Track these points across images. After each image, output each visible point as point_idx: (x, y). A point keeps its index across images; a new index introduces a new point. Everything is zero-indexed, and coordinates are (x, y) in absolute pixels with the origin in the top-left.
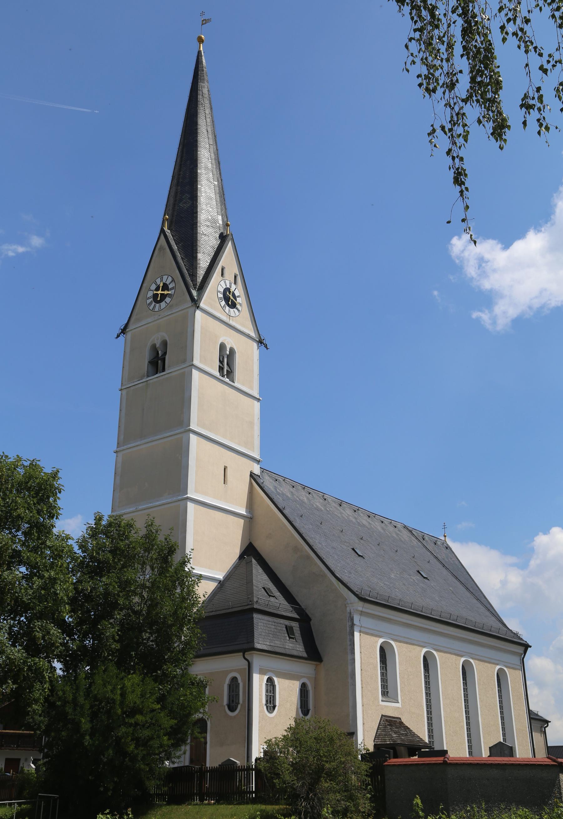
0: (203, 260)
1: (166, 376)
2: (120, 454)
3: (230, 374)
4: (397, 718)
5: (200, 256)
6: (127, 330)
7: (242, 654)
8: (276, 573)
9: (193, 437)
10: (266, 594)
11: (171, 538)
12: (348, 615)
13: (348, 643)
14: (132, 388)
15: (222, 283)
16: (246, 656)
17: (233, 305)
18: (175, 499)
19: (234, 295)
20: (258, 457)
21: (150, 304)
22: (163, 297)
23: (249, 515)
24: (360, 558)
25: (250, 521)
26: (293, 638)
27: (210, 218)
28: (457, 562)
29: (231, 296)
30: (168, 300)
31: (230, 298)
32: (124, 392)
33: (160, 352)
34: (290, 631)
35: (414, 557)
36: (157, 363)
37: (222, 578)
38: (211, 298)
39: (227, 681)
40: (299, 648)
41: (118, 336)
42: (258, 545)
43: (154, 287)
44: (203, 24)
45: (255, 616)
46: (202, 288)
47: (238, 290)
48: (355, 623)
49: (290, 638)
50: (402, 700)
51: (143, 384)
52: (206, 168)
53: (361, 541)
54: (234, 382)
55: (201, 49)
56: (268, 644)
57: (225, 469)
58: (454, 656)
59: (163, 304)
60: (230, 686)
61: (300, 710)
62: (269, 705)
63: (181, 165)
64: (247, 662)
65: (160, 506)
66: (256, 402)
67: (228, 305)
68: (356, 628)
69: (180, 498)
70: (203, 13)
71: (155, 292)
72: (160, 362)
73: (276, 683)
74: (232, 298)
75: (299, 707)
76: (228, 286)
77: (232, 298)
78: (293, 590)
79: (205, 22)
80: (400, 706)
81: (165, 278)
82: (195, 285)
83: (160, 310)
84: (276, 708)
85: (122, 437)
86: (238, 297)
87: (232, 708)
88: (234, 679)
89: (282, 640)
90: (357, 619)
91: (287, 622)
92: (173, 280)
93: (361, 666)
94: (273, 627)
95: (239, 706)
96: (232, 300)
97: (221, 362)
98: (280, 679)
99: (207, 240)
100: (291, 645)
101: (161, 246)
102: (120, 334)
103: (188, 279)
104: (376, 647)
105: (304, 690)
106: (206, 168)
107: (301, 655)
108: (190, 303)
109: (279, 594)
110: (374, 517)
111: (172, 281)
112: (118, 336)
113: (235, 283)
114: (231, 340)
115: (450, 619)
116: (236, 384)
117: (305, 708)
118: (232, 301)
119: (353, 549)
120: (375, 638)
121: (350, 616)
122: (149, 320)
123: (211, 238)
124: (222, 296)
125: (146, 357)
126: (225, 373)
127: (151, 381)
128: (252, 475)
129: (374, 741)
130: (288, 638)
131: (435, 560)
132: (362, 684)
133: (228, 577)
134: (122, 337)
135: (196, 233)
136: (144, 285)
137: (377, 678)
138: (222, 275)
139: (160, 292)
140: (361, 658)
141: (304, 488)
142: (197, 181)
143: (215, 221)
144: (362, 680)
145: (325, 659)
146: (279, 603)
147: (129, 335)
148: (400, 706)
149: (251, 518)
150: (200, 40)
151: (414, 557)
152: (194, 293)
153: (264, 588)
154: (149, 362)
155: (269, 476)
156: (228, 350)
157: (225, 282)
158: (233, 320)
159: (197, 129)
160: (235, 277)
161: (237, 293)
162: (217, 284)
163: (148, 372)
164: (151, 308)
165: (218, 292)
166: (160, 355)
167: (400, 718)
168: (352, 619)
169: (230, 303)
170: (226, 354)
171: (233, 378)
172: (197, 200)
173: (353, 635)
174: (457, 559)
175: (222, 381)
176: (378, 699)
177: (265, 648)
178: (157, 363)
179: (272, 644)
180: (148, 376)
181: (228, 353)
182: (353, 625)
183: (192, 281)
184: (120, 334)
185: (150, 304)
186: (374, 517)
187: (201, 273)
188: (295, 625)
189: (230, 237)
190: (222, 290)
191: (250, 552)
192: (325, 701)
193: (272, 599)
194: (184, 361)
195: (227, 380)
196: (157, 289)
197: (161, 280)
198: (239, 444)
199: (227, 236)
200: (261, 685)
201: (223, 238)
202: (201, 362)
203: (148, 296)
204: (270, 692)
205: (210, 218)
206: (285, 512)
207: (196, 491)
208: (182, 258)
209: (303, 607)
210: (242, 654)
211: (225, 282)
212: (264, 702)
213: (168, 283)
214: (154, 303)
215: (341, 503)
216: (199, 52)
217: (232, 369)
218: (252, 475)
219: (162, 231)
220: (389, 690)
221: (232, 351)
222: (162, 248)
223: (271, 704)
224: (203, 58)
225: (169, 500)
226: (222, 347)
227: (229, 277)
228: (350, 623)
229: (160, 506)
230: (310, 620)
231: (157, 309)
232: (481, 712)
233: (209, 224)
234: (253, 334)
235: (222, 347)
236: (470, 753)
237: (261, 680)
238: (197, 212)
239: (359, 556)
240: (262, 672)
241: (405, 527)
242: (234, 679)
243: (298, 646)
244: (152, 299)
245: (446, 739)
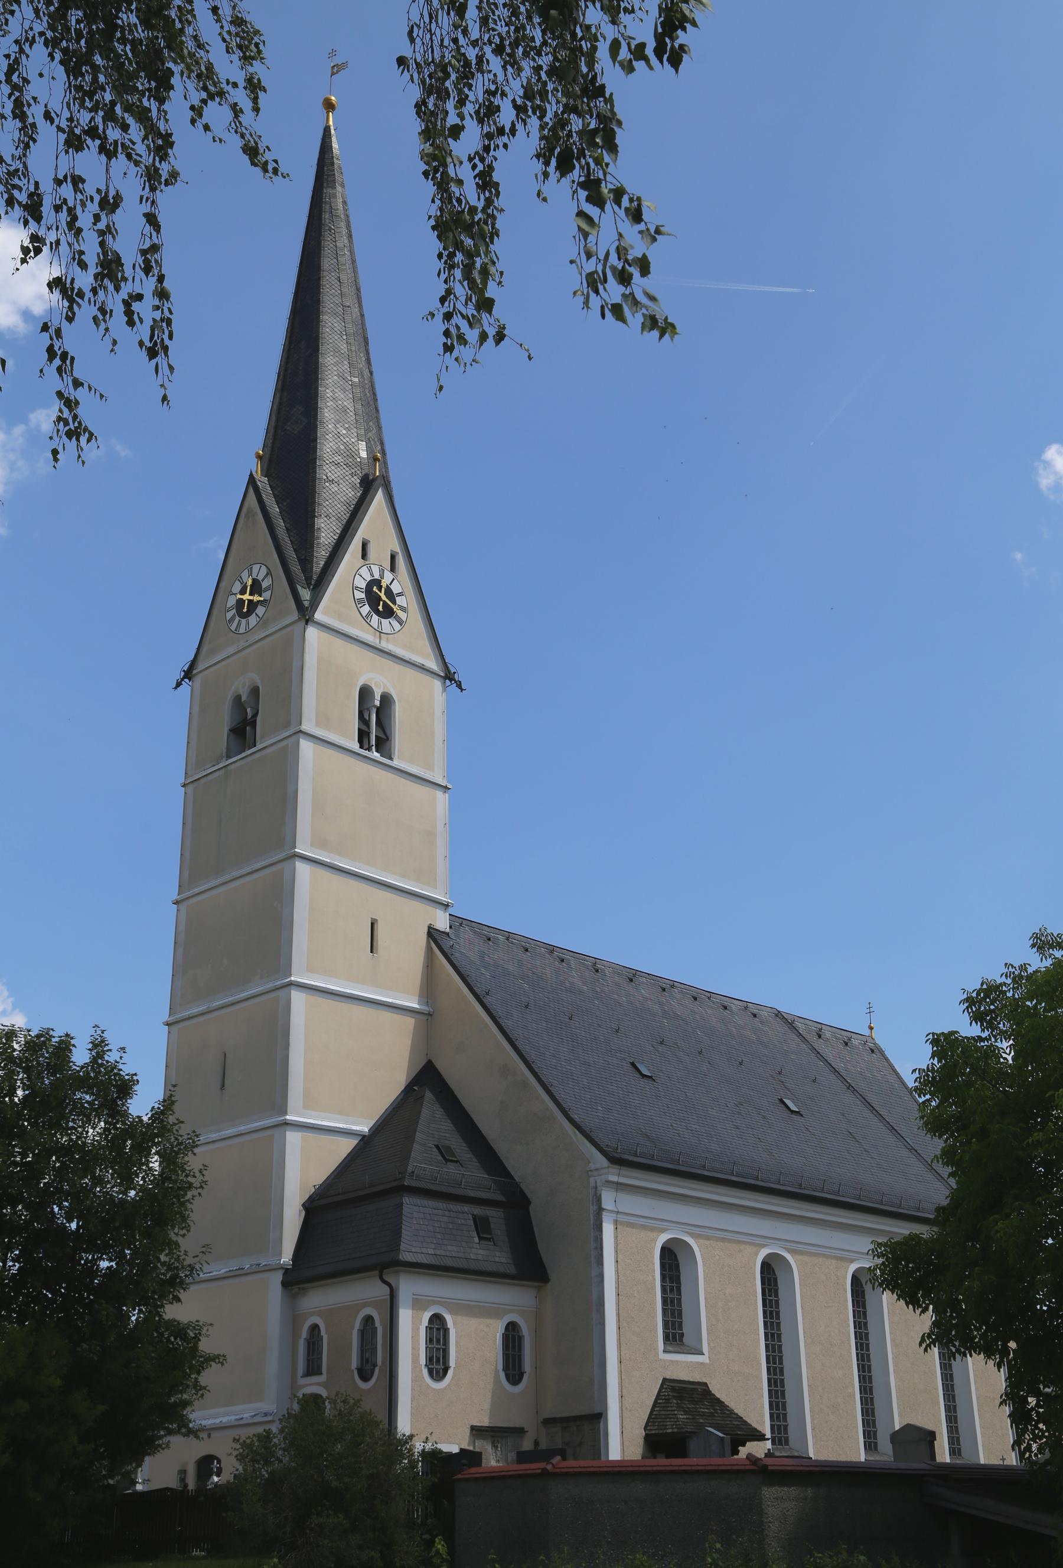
0: (327, 530)
1: (258, 755)
2: (184, 907)
3: (383, 744)
4: (699, 1383)
5: (320, 523)
6: (194, 672)
7: (377, 1272)
8: (473, 1116)
9: (301, 867)
10: (440, 1158)
11: (121, 1066)
12: (592, 1192)
13: (593, 1244)
14: (202, 781)
15: (364, 571)
16: (385, 1278)
17: (388, 613)
18: (270, 986)
19: (389, 592)
20: (444, 899)
21: (232, 619)
22: (253, 606)
23: (425, 1008)
24: (643, 1082)
25: (428, 1019)
26: (488, 1239)
27: (342, 447)
28: (892, 1078)
29: (382, 595)
30: (260, 610)
31: (380, 598)
32: (190, 788)
33: (249, 710)
34: (482, 1226)
35: (780, 1073)
36: (243, 731)
37: (367, 1130)
38: (340, 599)
39: (357, 1325)
40: (500, 1257)
41: (178, 684)
42: (442, 1066)
43: (237, 587)
44: (333, 74)
45: (406, 1199)
46: (319, 584)
47: (399, 583)
48: (604, 1206)
49: (480, 1238)
50: (711, 1349)
51: (223, 771)
52: (337, 352)
53: (661, 1048)
54: (391, 759)
55: (331, 123)
56: (431, 1251)
57: (372, 925)
58: (834, 1262)
59: (253, 620)
60: (362, 1332)
61: (502, 1375)
62: (434, 1366)
63: (289, 350)
64: (387, 1289)
65: (247, 999)
66: (439, 794)
67: (378, 612)
68: (605, 1216)
69: (278, 983)
70: (333, 53)
71: (239, 596)
72: (245, 727)
73: (450, 1324)
74: (384, 597)
75: (500, 1366)
76: (377, 576)
77: (384, 597)
78: (502, 1147)
79: (336, 69)
80: (707, 1361)
81: (256, 568)
82: (308, 579)
83: (249, 631)
84: (450, 1372)
85: (186, 873)
86: (400, 594)
87: (365, 1376)
88: (369, 1319)
89: (464, 1244)
90: (608, 1199)
91: (477, 1210)
92: (269, 573)
93: (617, 1288)
94: (445, 1219)
95: (377, 1370)
96: (384, 602)
97: (363, 719)
98: (459, 1318)
99: (335, 488)
100: (481, 1252)
101: (249, 509)
102: (182, 680)
103: (296, 568)
104: (651, 1251)
105: (514, 1336)
106: (337, 352)
107: (502, 1270)
108: (295, 616)
109: (470, 1156)
110: (709, 998)
111: (267, 574)
112: (178, 684)
113: (393, 569)
114: (382, 679)
115: (822, 1191)
116: (396, 763)
117: (514, 1369)
118: (385, 604)
119: (633, 1064)
120: (649, 1234)
121: (596, 1194)
122: (231, 650)
123: (344, 486)
124: (363, 596)
125: (225, 721)
126: (373, 742)
127: (233, 767)
128: (432, 934)
129: (645, 1429)
130: (476, 1240)
131: (832, 1077)
132: (619, 1321)
133: (379, 1129)
134: (186, 687)
135: (314, 479)
136: (223, 584)
137: (655, 1309)
138: (364, 556)
139: (246, 597)
140: (617, 1271)
141: (552, 952)
142: (317, 379)
143: (352, 454)
144: (618, 1315)
145: (553, 1275)
146: (470, 1174)
147: (198, 680)
148: (707, 1361)
149: (430, 1014)
150: (329, 106)
151: (780, 1073)
152: (305, 594)
153: (437, 1147)
154: (231, 730)
155: (475, 932)
156: (378, 697)
157: (370, 570)
158: (388, 640)
159: (319, 279)
160: (393, 557)
161: (396, 588)
162: (350, 574)
163: (228, 749)
164: (233, 628)
165: (355, 588)
166: (249, 716)
167: (706, 1384)
168: (598, 1200)
169: (380, 608)
170: (375, 706)
171: (390, 750)
172: (316, 414)
173: (599, 1228)
174: (894, 1070)
175: (365, 757)
176: (656, 1348)
177: (422, 1259)
178: (243, 731)
179: (438, 1252)
180: (228, 757)
181: (377, 703)
182: (600, 1210)
183: (304, 571)
184: (182, 680)
185: (232, 619)
186: (709, 998)
187: (321, 555)
188: (496, 1216)
189: (380, 481)
190: (363, 585)
191: (427, 1080)
192: (552, 1358)
193: (451, 1168)
194: (287, 725)
195: (376, 755)
196: (243, 592)
197: (250, 574)
198: (403, 876)
199: (375, 479)
200: (415, 1330)
201: (368, 485)
202: (318, 724)
203: (229, 605)
204: (438, 1341)
205: (342, 447)
206: (487, 1000)
207: (310, 969)
208: (287, 529)
209: (517, 1179)
210: (377, 1272)
211: (370, 570)
212: (423, 1360)
213: (260, 578)
214: (237, 618)
215: (634, 975)
216: (327, 129)
217: (388, 734)
218: (432, 934)
219: (252, 480)
220: (684, 1331)
221: (386, 699)
222: (250, 514)
223: (437, 1364)
224: (334, 139)
225: (261, 989)
226: (365, 693)
227: (379, 554)
228: (595, 1208)
229: (247, 999)
230: (529, 1202)
231: (242, 630)
232: (896, 1365)
233: (338, 459)
234: (433, 664)
235: (365, 693)
236: (955, 1451)
237: (416, 1322)
238: (315, 440)
239: (644, 1076)
240: (419, 1304)
241: (778, 1014)
242: (369, 1319)
243: (498, 1254)
244: (234, 611)
245: (813, 1420)
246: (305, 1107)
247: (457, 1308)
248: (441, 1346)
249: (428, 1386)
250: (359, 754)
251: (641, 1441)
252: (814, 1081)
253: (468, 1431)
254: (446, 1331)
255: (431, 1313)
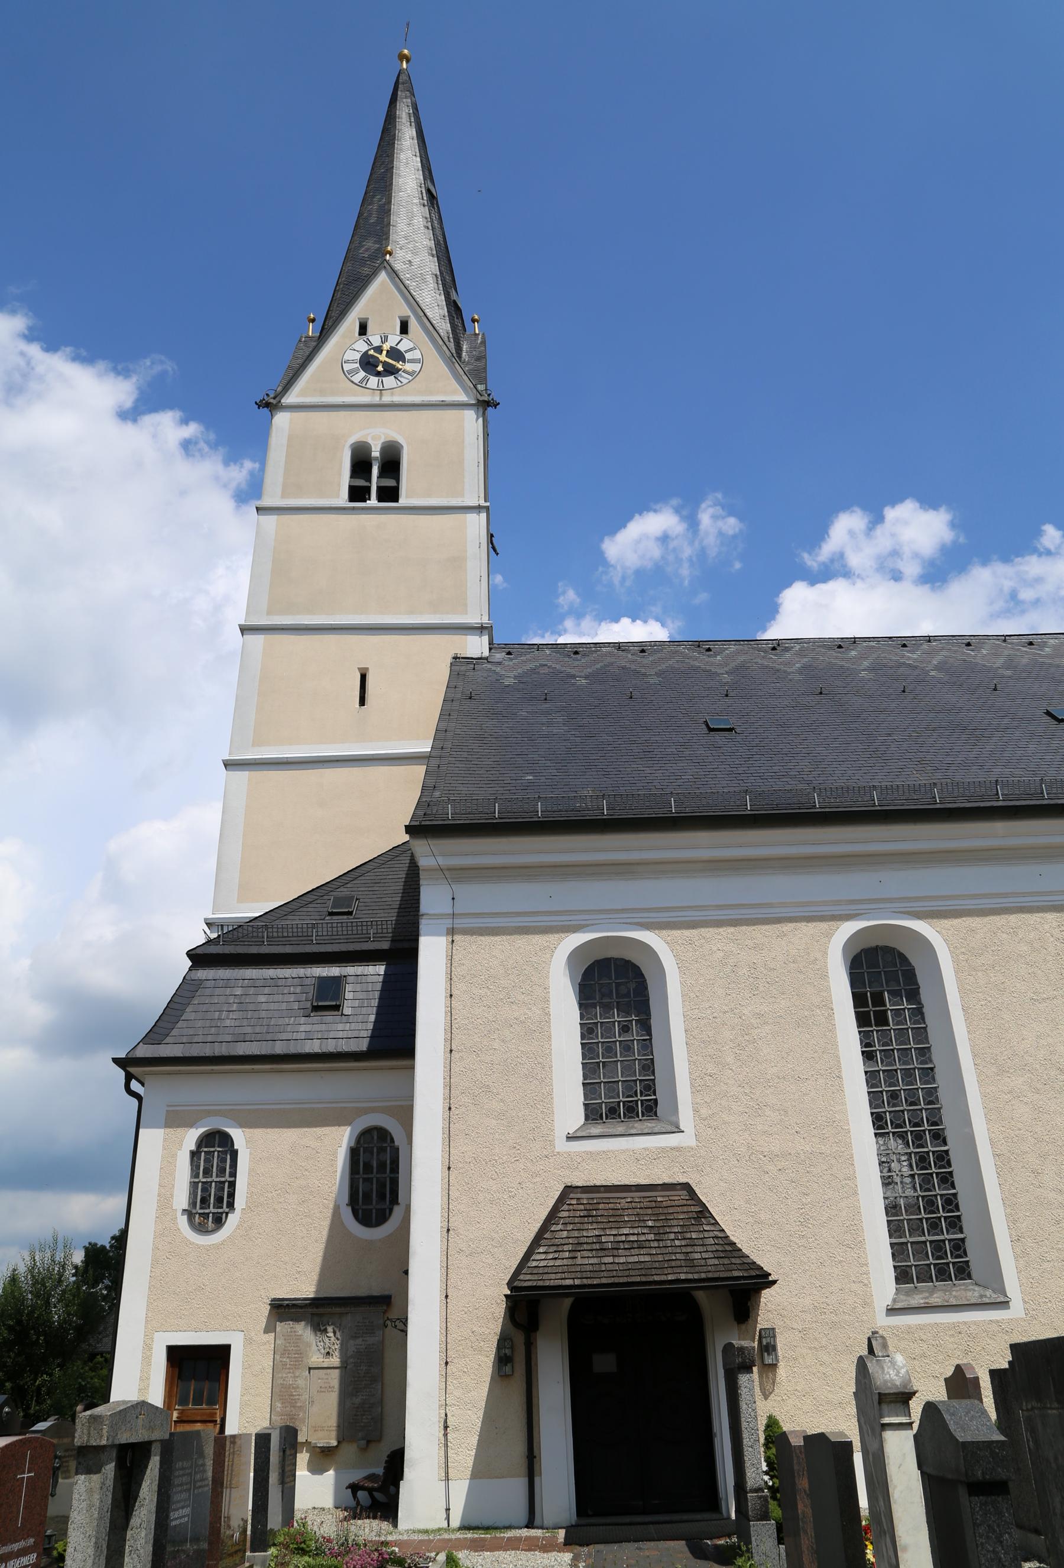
57: (363, 678)
61: (347, 1213)
80: (693, 1142)
148: (693, 1142)
175: (363, 508)
245: (1012, 1221)
246: (241, 900)
247: (253, 1119)
248: (227, 1178)
249: (217, 1247)
250: (354, 508)
251: (499, 1309)
252: (995, 689)
253: (266, 1309)
254: (234, 1154)
255: (201, 1130)
